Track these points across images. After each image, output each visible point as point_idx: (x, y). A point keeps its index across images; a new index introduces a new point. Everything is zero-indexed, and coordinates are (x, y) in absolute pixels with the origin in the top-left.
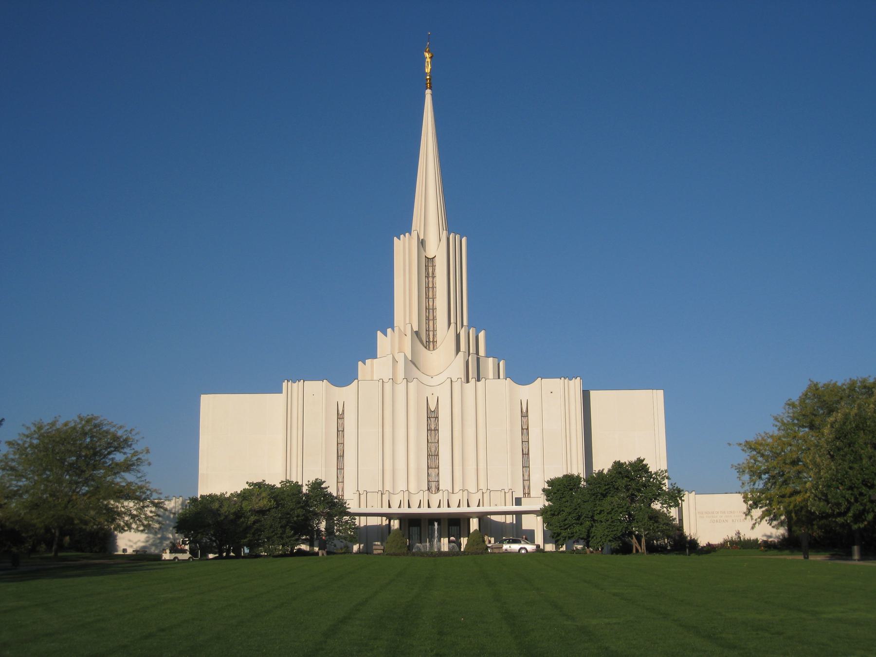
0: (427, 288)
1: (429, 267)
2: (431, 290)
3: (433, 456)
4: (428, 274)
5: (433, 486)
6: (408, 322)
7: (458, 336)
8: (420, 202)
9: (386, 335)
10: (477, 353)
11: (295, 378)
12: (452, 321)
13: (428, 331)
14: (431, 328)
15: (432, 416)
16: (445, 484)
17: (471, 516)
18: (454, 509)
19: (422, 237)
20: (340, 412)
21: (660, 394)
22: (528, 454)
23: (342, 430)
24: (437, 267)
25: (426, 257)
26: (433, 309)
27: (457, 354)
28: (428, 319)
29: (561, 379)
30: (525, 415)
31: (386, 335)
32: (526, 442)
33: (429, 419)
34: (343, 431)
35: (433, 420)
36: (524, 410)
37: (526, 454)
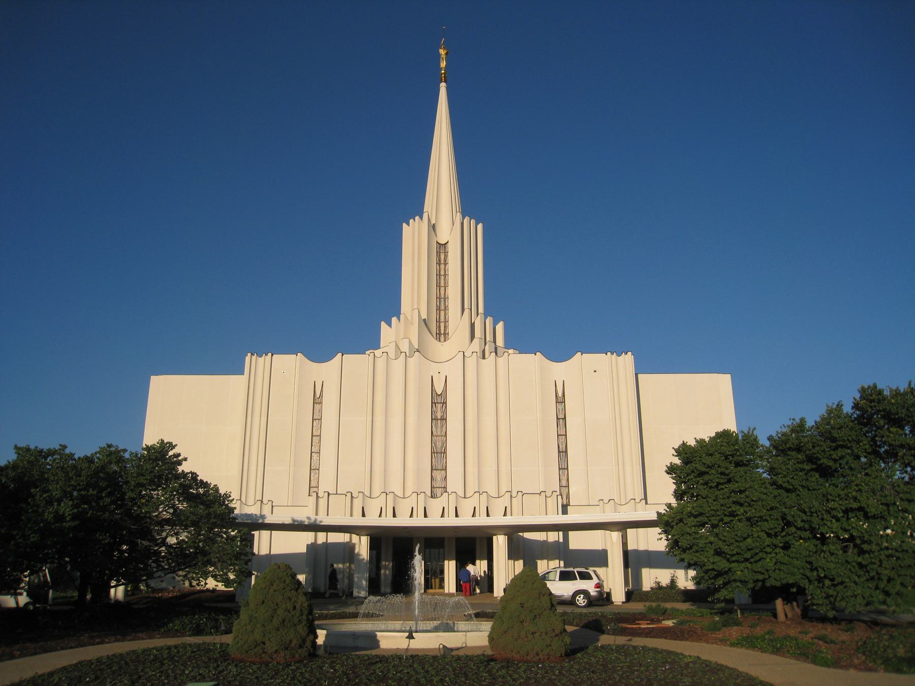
0: (438, 276)
1: (441, 254)
2: (442, 278)
3: (439, 453)
4: (440, 261)
5: (437, 489)
6: (415, 307)
7: (472, 326)
8: (431, 203)
9: (390, 325)
10: (495, 342)
11: (260, 353)
12: (466, 306)
13: (438, 321)
14: (442, 319)
15: (439, 400)
16: (454, 482)
17: (494, 532)
18: (465, 520)
19: (433, 222)
20: (318, 395)
21: (727, 378)
22: (566, 452)
23: (563, 417)
24: (449, 253)
25: (437, 242)
26: (445, 299)
27: (472, 341)
28: (438, 309)
29: (606, 354)
30: (561, 400)
31: (390, 325)
32: (562, 435)
33: (434, 405)
34: (565, 418)
35: (439, 406)
36: (560, 394)
37: (563, 453)
